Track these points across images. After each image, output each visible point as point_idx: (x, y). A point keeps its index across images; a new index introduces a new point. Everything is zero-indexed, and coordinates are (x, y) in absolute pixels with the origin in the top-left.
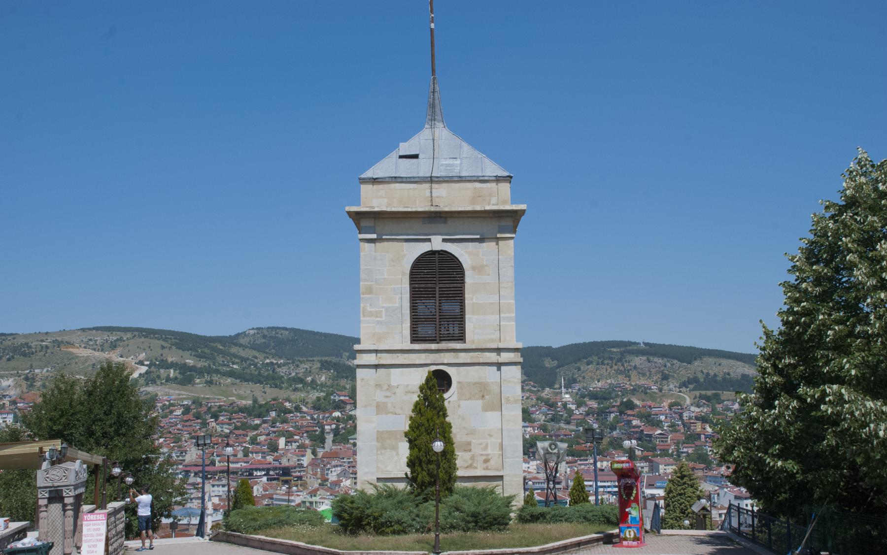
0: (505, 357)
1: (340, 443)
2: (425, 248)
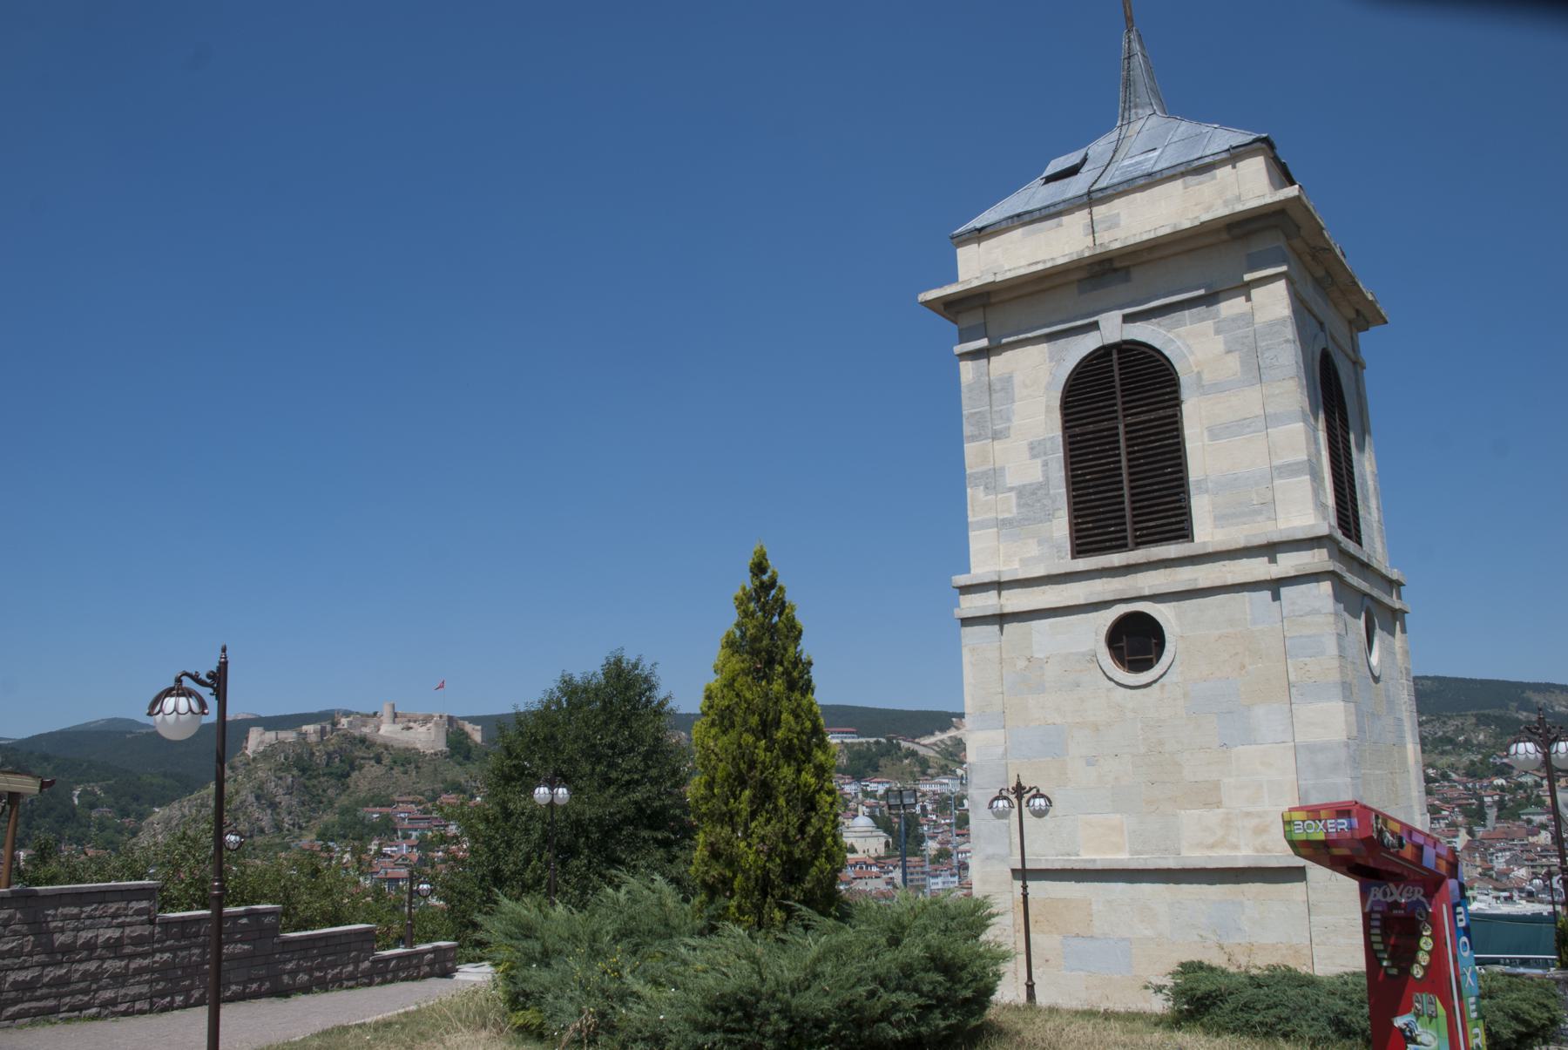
0: (1288, 563)
1: (1507, 819)
2: (1088, 343)
